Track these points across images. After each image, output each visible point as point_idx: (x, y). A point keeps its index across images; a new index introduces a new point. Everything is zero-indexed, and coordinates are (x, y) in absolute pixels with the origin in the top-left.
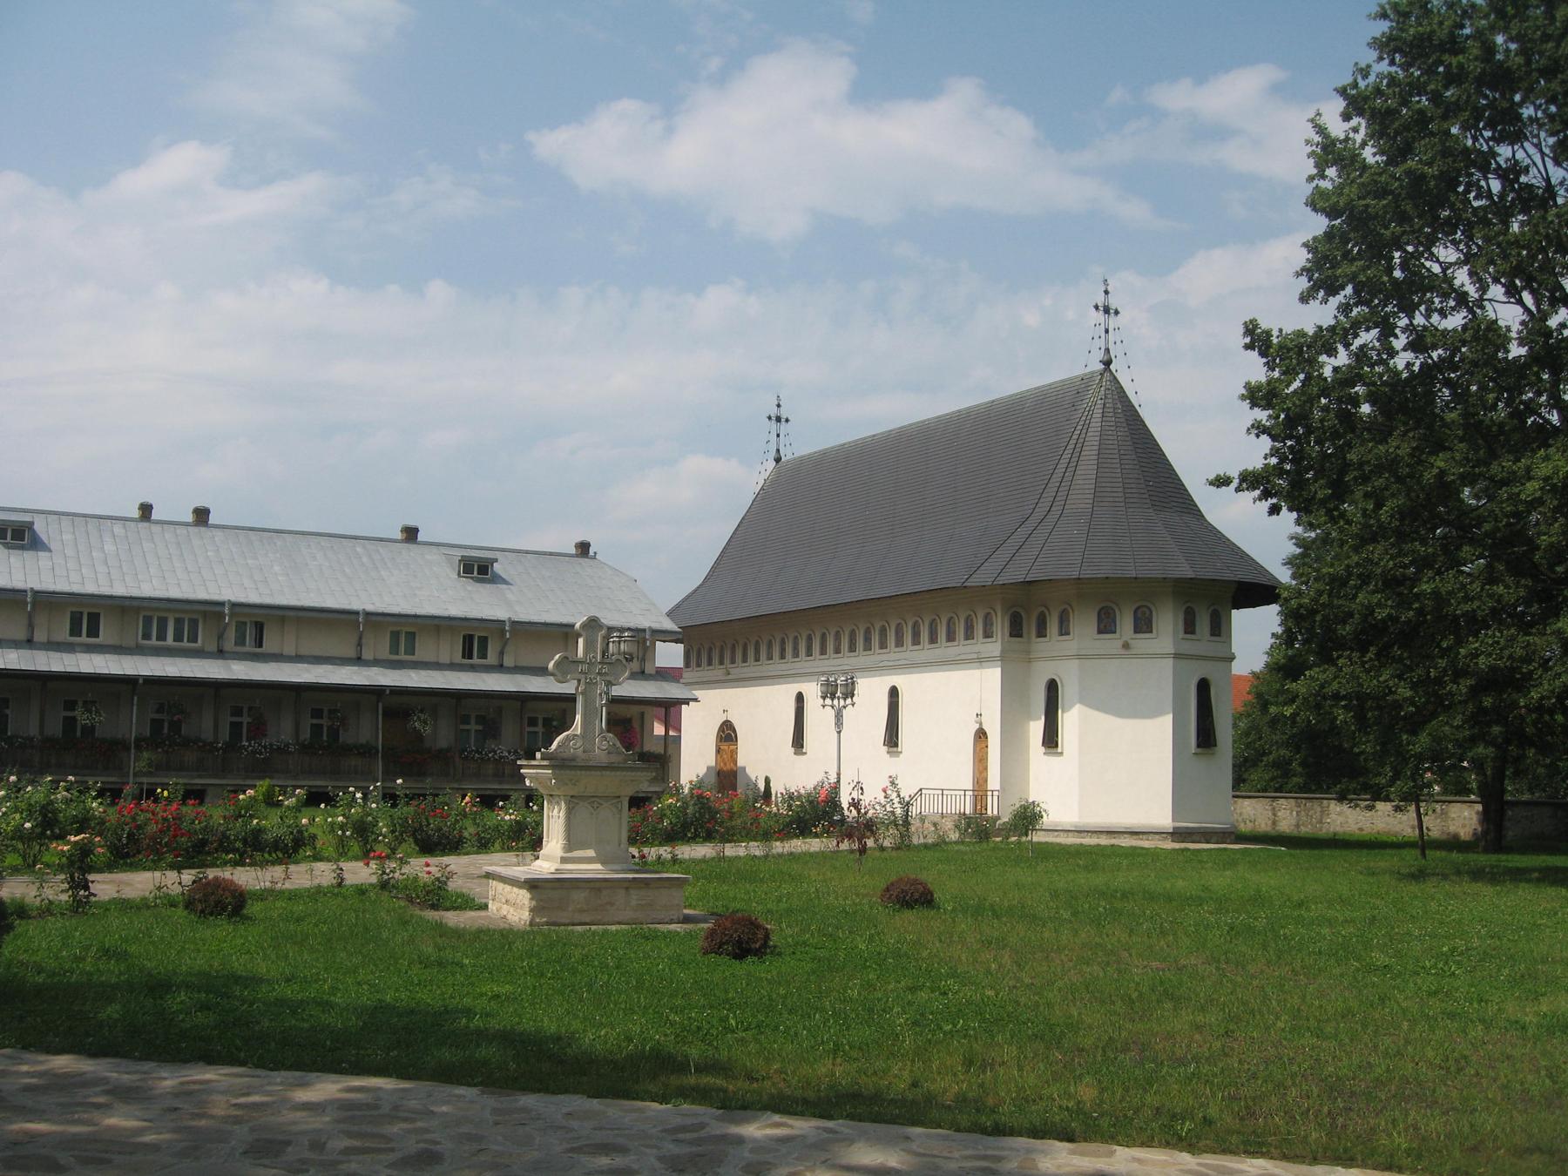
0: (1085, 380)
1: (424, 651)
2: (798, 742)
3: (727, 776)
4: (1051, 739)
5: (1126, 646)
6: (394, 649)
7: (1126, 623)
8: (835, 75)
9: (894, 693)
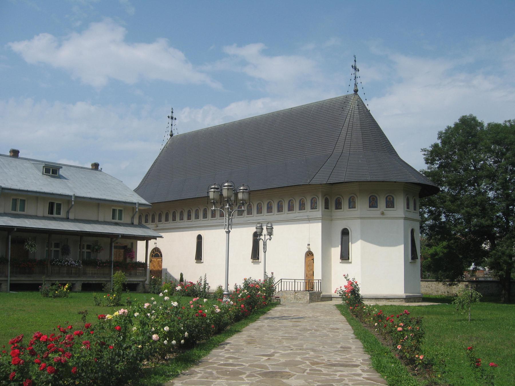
0: (346, 100)
1: (29, 209)
2: (199, 257)
4: (345, 256)
5: (383, 214)
6: (14, 208)
7: (382, 203)
8: (120, 32)
9: (199, 238)
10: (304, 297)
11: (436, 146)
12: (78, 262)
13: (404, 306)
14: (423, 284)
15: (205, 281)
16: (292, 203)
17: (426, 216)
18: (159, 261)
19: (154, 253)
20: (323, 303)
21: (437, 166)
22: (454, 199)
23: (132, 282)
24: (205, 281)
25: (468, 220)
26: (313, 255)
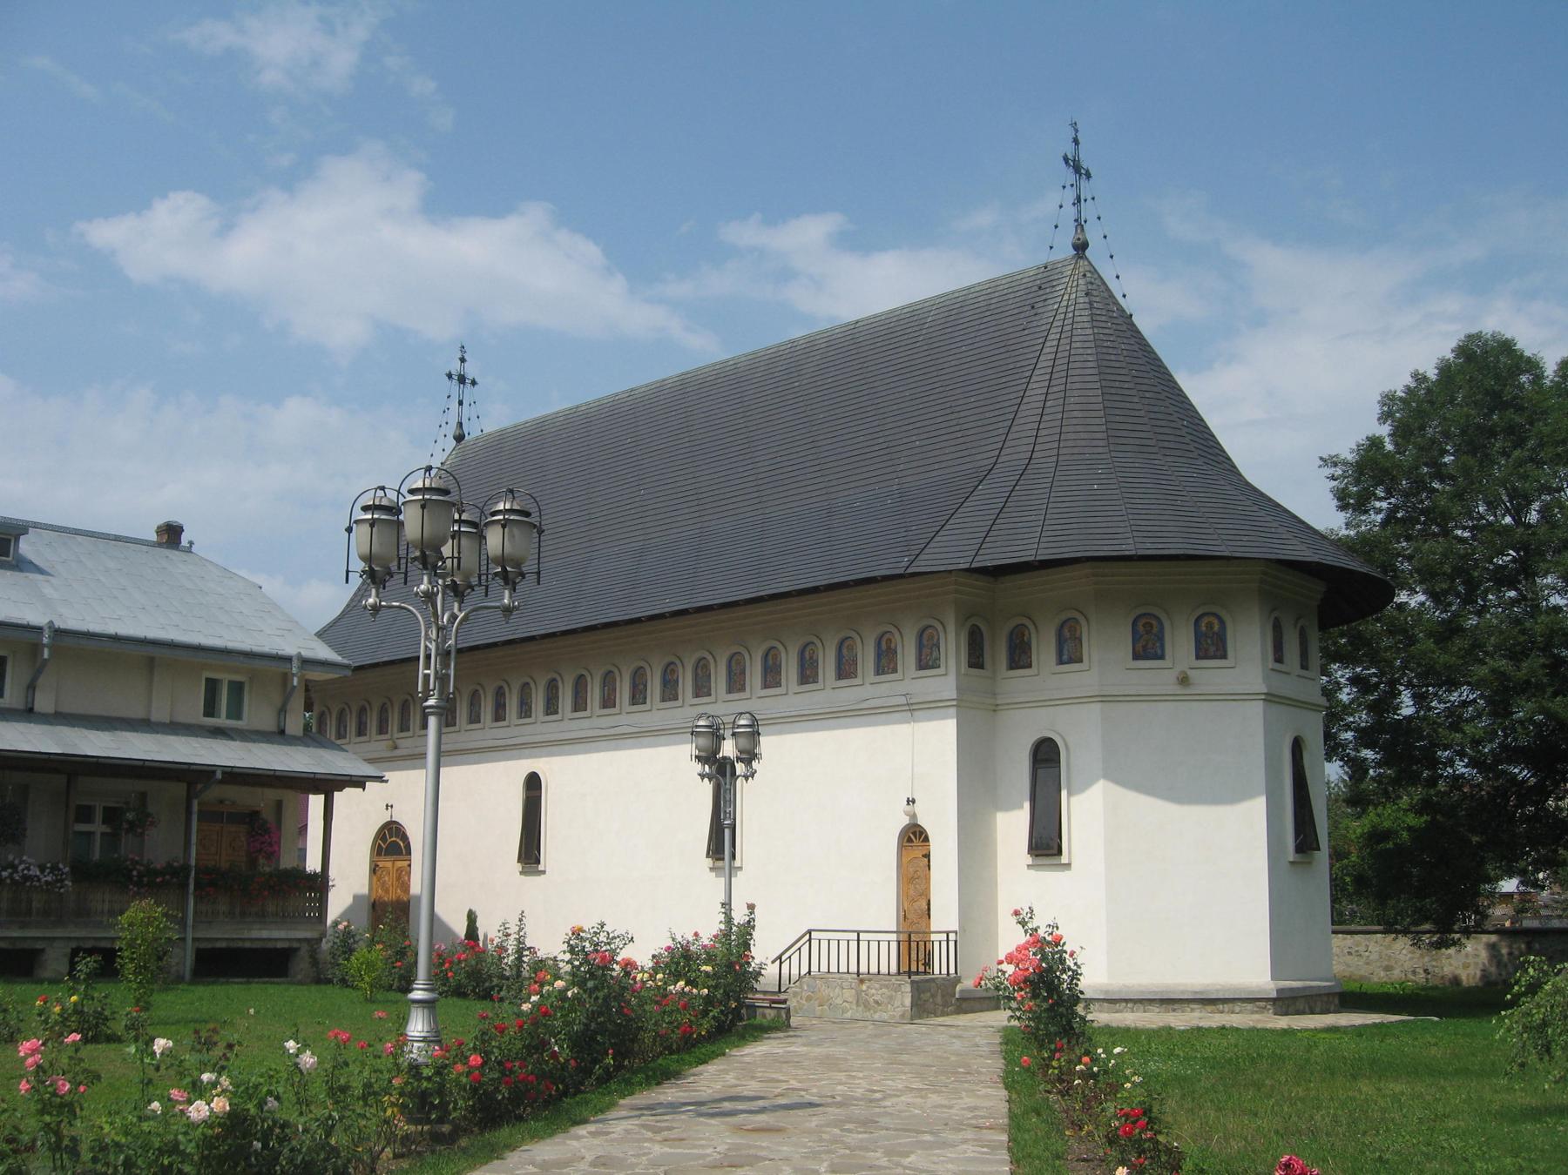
0: (1043, 282)
2: (530, 852)
3: (390, 912)
4: (1046, 844)
5: (1184, 680)
7: (1180, 643)
8: (409, 187)
9: (533, 784)
10: (891, 997)
11: (1375, 443)
12: (54, 869)
13: (1272, 1031)
14: (1340, 942)
15: (520, 941)
16: (851, 648)
17: (1344, 696)
18: (400, 870)
19: (384, 839)
20: (963, 1020)
21: (1379, 518)
22: (1449, 631)
23: (270, 945)
24: (520, 941)
25: (1500, 707)
26: (926, 839)
